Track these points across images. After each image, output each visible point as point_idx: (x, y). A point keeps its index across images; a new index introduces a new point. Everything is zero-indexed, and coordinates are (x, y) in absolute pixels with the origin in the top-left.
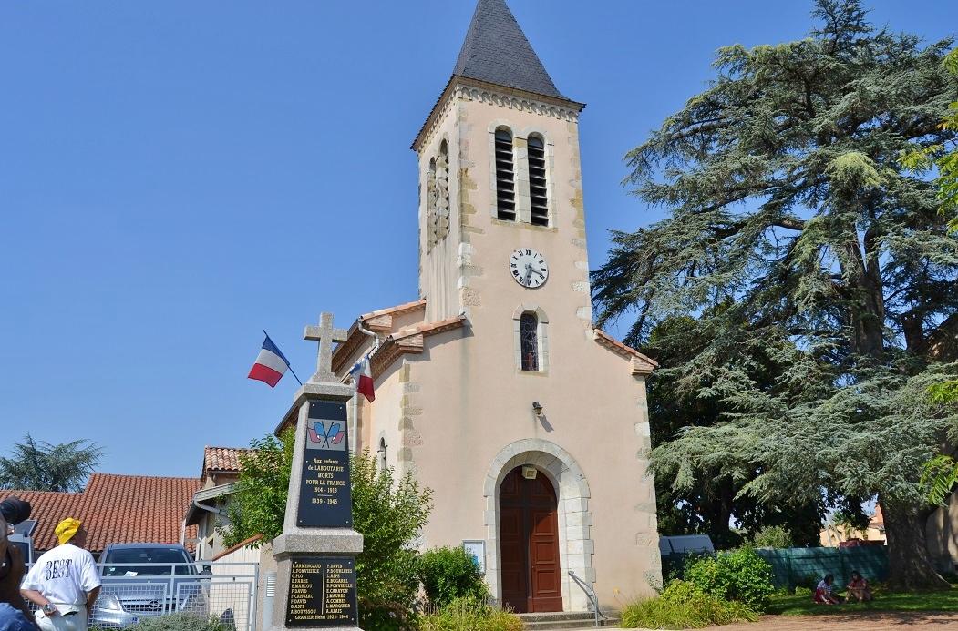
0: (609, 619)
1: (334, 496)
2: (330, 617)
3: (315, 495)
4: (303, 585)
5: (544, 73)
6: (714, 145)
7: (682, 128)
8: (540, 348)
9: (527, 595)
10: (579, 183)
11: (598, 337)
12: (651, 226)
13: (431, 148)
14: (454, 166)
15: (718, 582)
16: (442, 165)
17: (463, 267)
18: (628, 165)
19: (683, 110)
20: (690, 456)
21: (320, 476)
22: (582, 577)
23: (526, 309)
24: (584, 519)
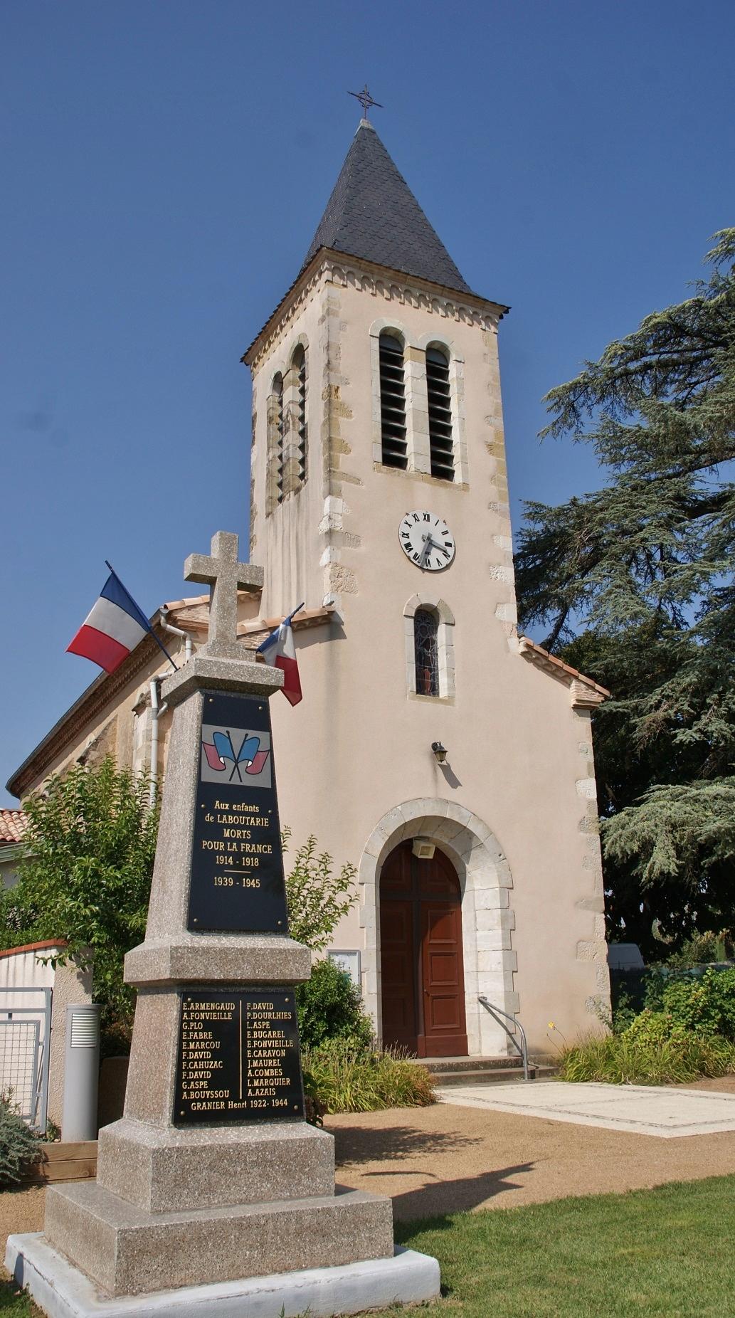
0: (542, 1067)
1: (254, 873)
2: (255, 1104)
3: (220, 871)
4: (203, 1043)
5: (446, 258)
6: (670, 389)
7: (631, 360)
8: (442, 662)
9: (416, 1033)
10: (499, 421)
11: (525, 649)
12: (588, 496)
13: (276, 357)
14: (315, 384)
15: (705, 1014)
16: (293, 383)
17: (330, 533)
18: (549, 410)
19: (638, 333)
20: (669, 828)
21: (227, 834)
22: (498, 1002)
23: (424, 602)
24: (504, 920)
